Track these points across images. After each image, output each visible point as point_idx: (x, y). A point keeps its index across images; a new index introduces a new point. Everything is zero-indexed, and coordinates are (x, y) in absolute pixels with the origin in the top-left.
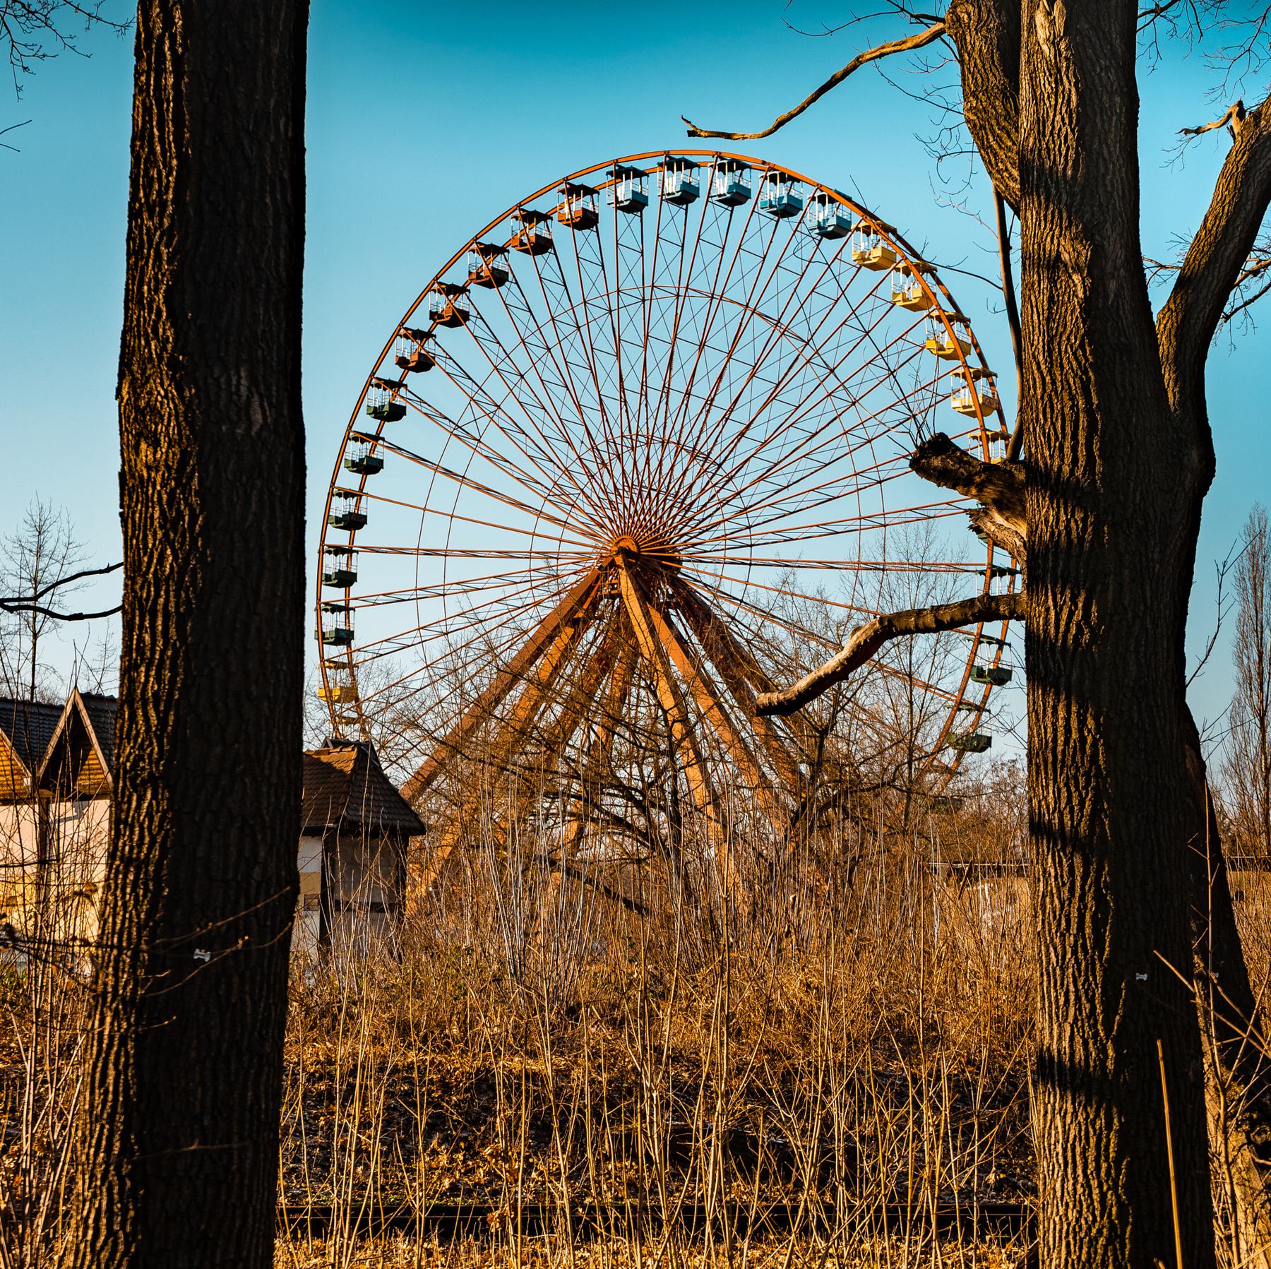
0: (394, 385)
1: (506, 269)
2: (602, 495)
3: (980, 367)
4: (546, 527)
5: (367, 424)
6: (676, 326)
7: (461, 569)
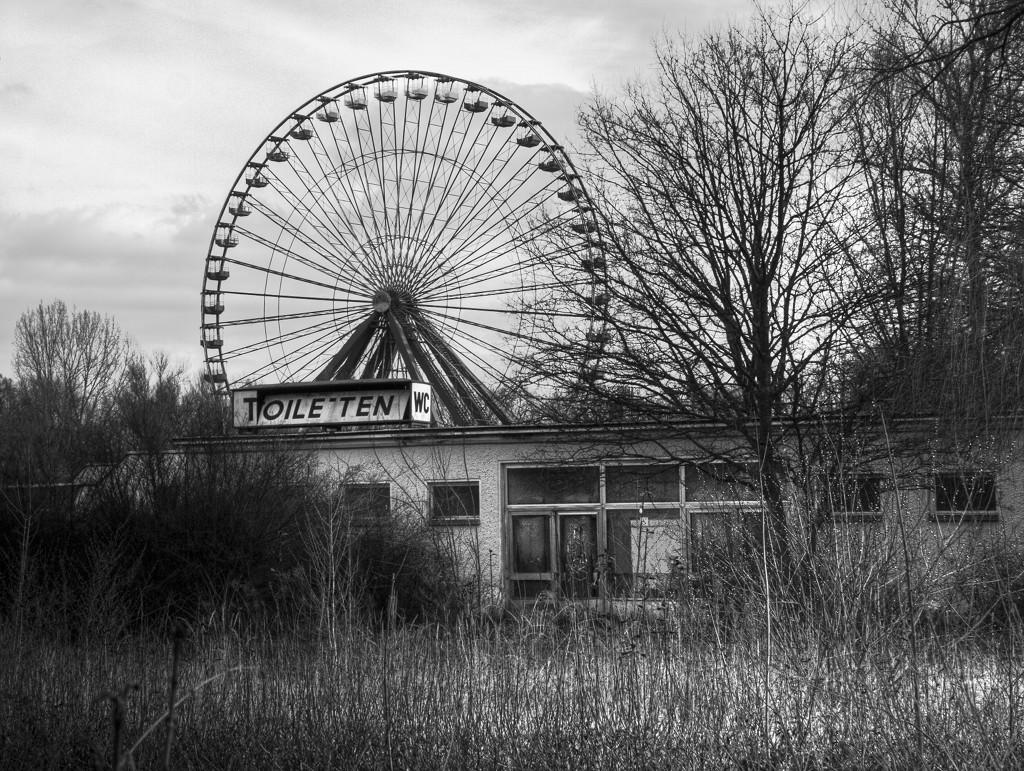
0: (243, 195)
1: (311, 129)
2: (375, 268)
3: (573, 173)
4: (340, 295)
5: (228, 218)
6: (370, 205)
7: (438, 225)
